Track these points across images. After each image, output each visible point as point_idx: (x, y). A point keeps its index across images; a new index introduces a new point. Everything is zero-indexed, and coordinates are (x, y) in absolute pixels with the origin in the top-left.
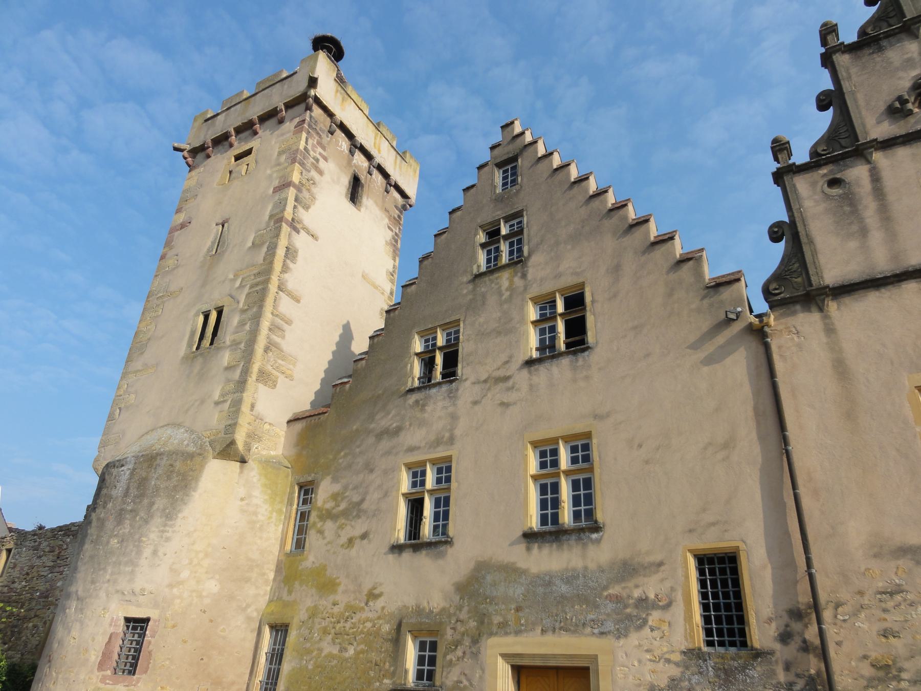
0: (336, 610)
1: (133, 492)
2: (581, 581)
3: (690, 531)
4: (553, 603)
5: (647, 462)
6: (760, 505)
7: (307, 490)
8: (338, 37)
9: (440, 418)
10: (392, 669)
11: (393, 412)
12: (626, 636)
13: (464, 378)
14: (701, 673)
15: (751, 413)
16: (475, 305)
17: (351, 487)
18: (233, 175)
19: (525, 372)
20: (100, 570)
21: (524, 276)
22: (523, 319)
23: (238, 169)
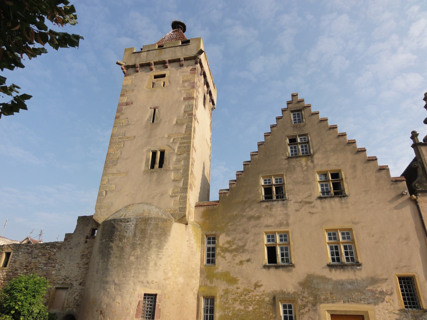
0: (239, 291)
1: (139, 235)
2: (356, 284)
3: (396, 268)
4: (343, 291)
5: (376, 242)
6: (421, 261)
7: (212, 239)
8: (186, 24)
9: (280, 215)
10: (274, 315)
11: (255, 209)
12: (378, 304)
13: (290, 199)
14: (406, 317)
15: (414, 229)
16: (291, 170)
17: (237, 239)
18: (155, 85)
19: (319, 201)
20: (127, 271)
21: (312, 162)
22: (314, 180)
23: (158, 83)
